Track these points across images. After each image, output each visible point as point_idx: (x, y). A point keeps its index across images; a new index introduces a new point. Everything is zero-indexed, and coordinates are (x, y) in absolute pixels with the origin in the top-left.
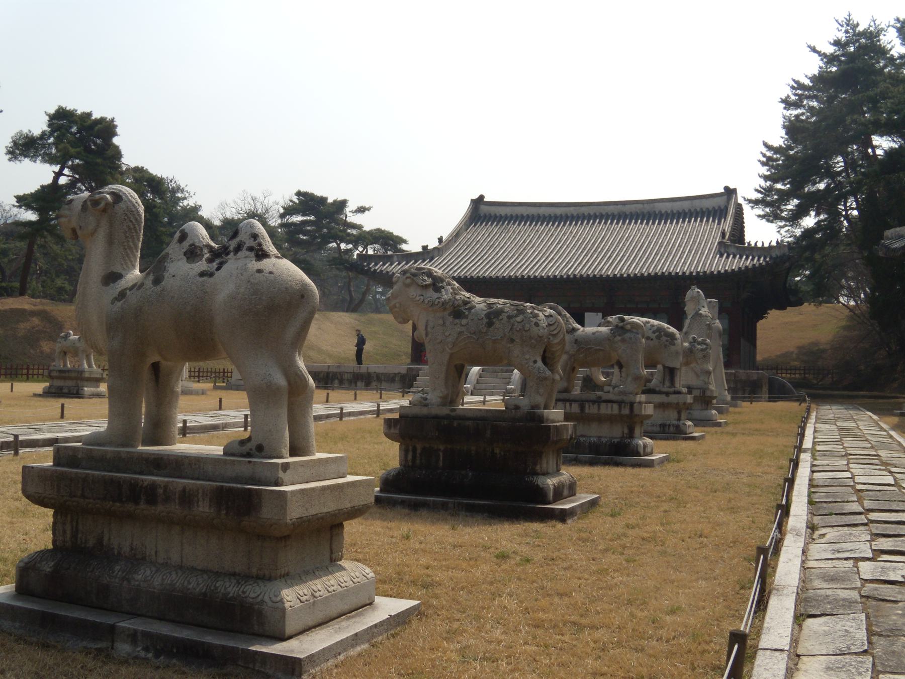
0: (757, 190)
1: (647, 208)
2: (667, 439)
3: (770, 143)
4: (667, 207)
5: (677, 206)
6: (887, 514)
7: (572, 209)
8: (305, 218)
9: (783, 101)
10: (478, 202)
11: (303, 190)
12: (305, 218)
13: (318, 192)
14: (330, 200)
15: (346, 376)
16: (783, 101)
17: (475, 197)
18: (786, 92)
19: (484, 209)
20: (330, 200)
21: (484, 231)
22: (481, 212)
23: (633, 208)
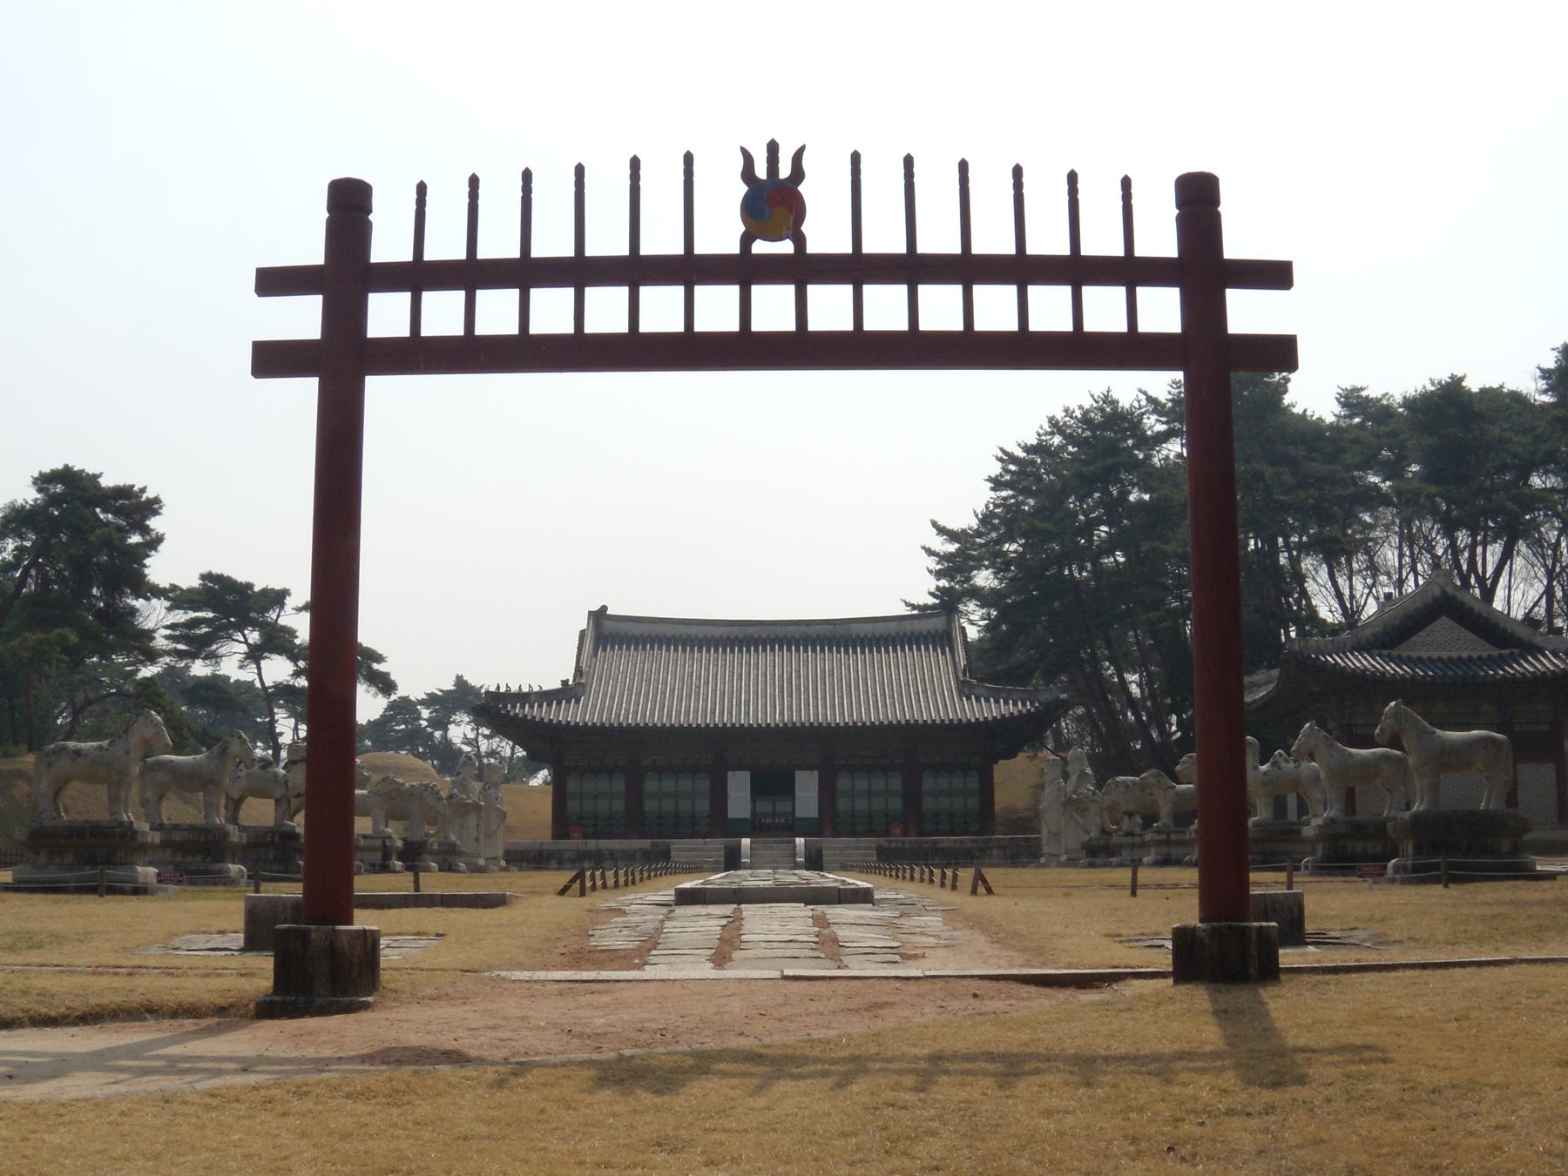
0: (932, 594)
1: (840, 629)
2: (1450, 880)
3: (942, 523)
4: (867, 629)
5: (880, 629)
6: (578, 977)
7: (736, 629)
8: (192, 615)
9: (990, 479)
10: (599, 617)
11: (216, 570)
12: (192, 615)
13: (241, 577)
14: (257, 589)
15: (567, 855)
16: (990, 479)
17: (595, 608)
18: (996, 469)
19: (609, 626)
20: (257, 589)
21: (622, 661)
22: (607, 633)
23: (821, 630)
